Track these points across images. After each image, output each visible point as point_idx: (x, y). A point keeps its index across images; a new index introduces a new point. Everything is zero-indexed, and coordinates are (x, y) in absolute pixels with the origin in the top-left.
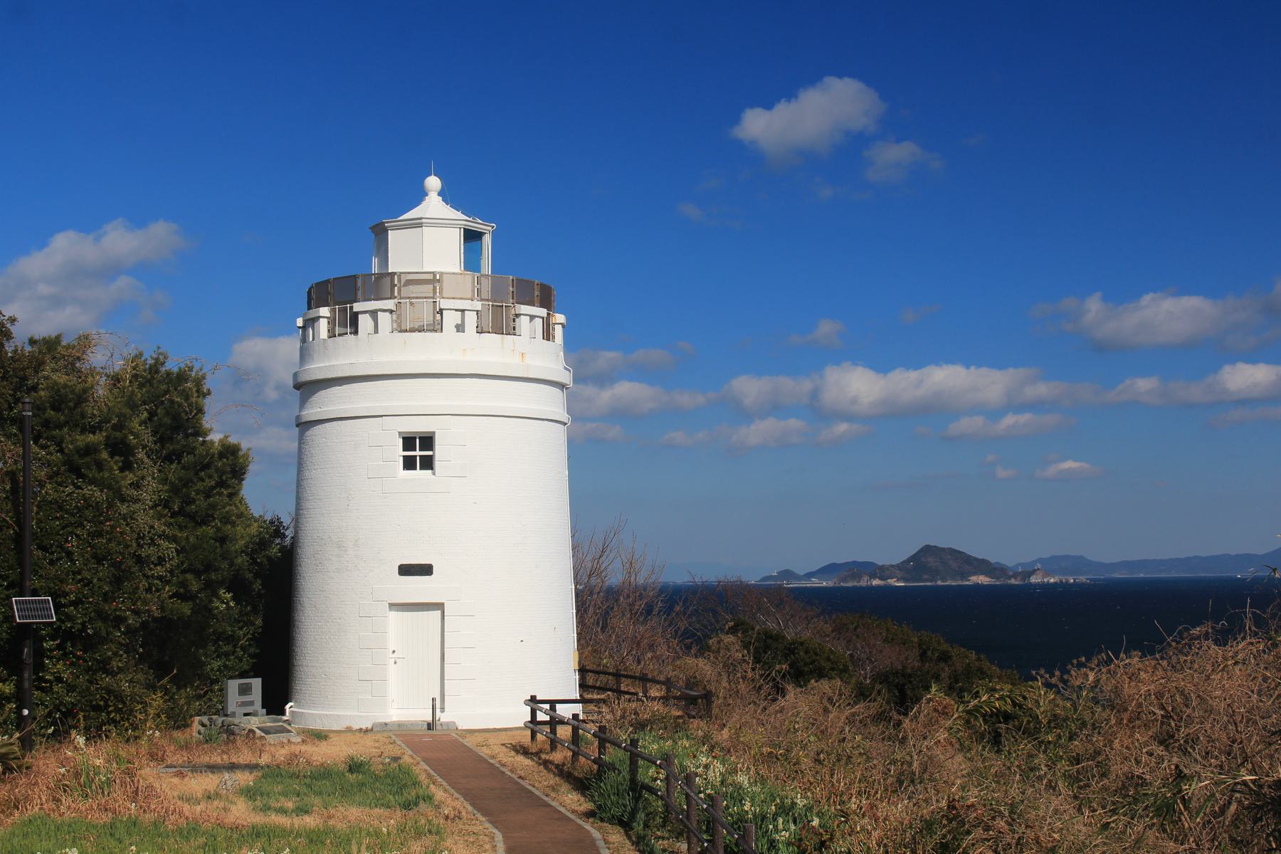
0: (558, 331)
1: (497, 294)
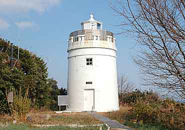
0: (114, 41)
1: (103, 32)
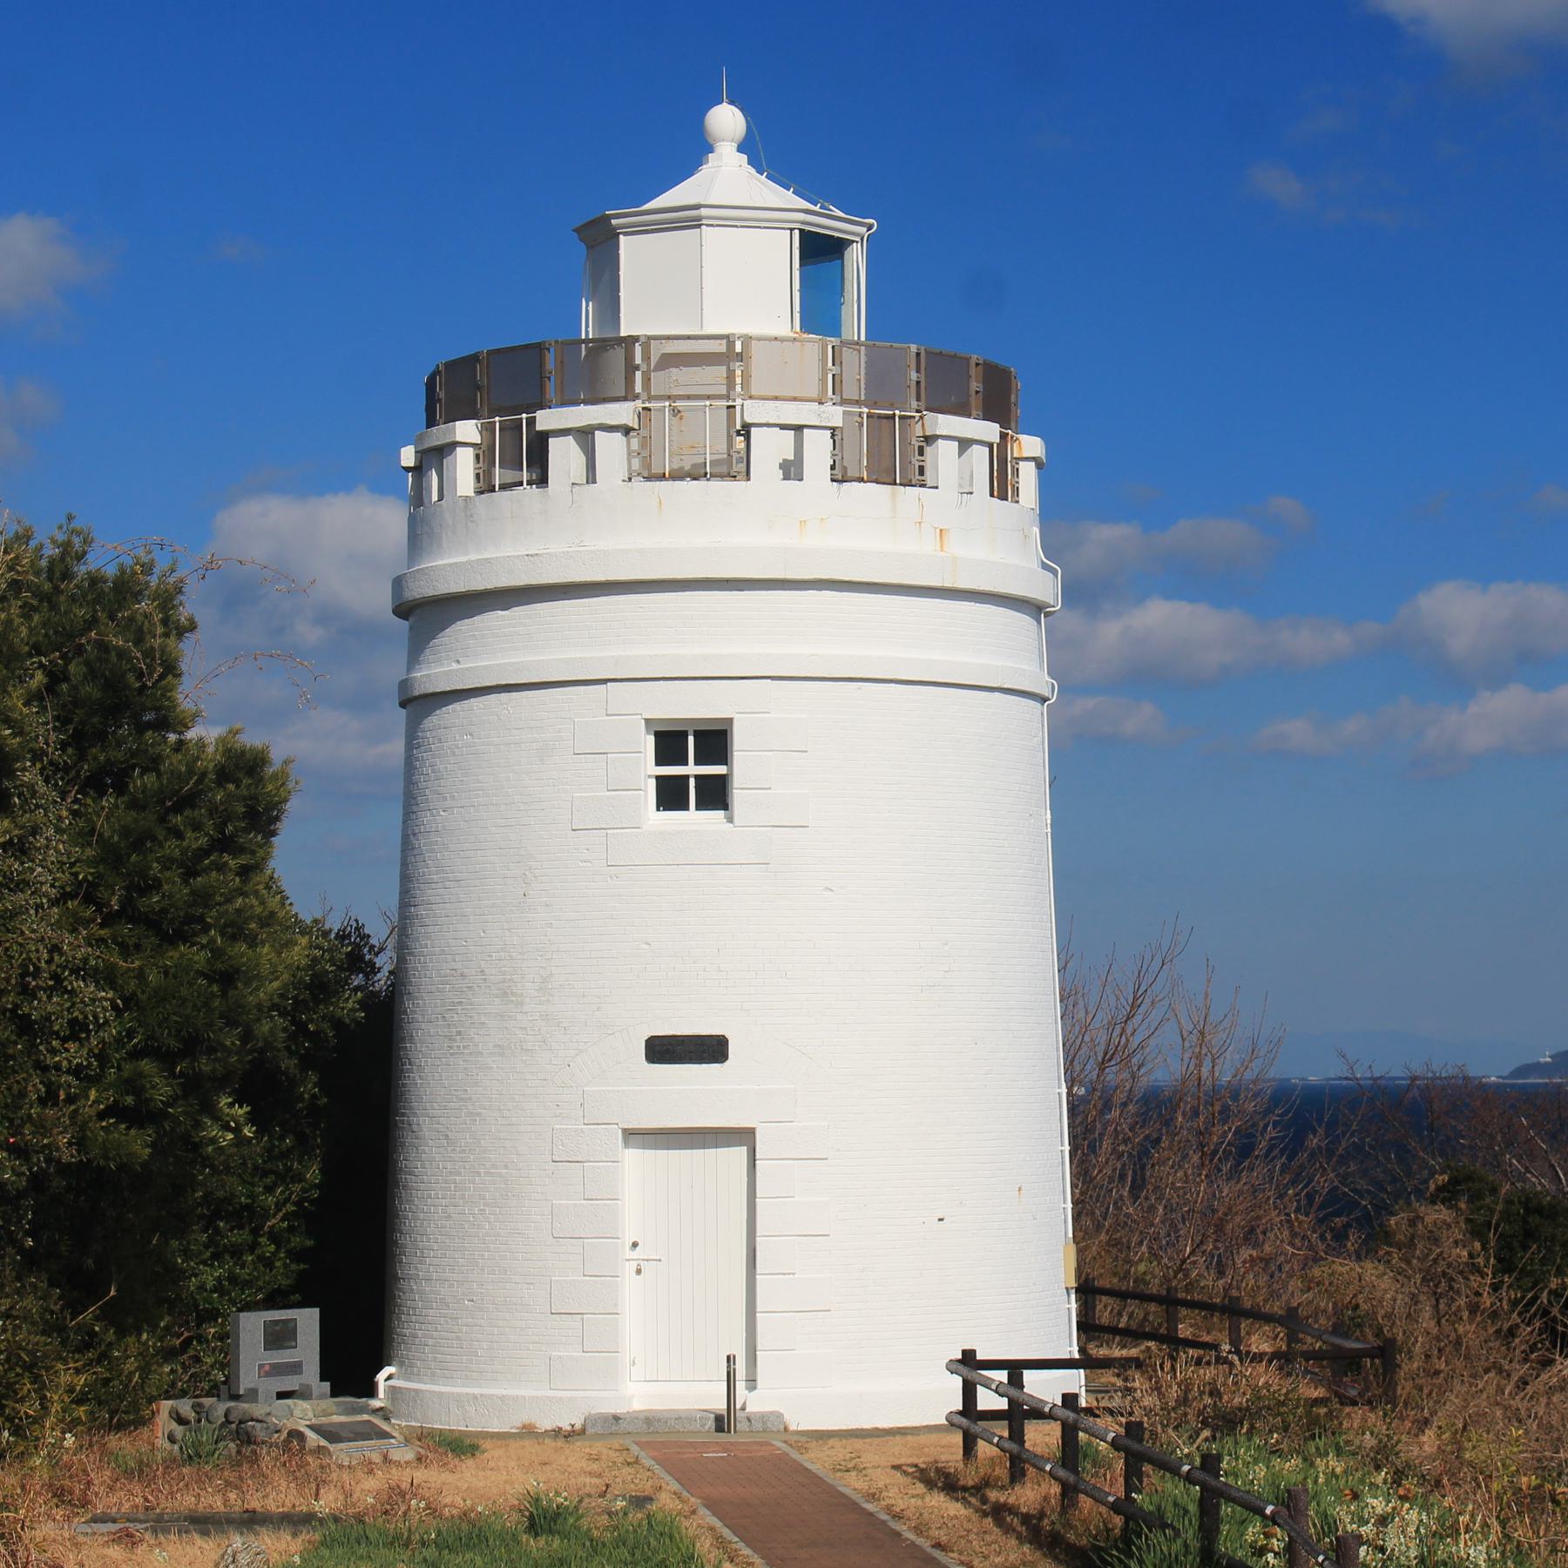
0: (1028, 477)
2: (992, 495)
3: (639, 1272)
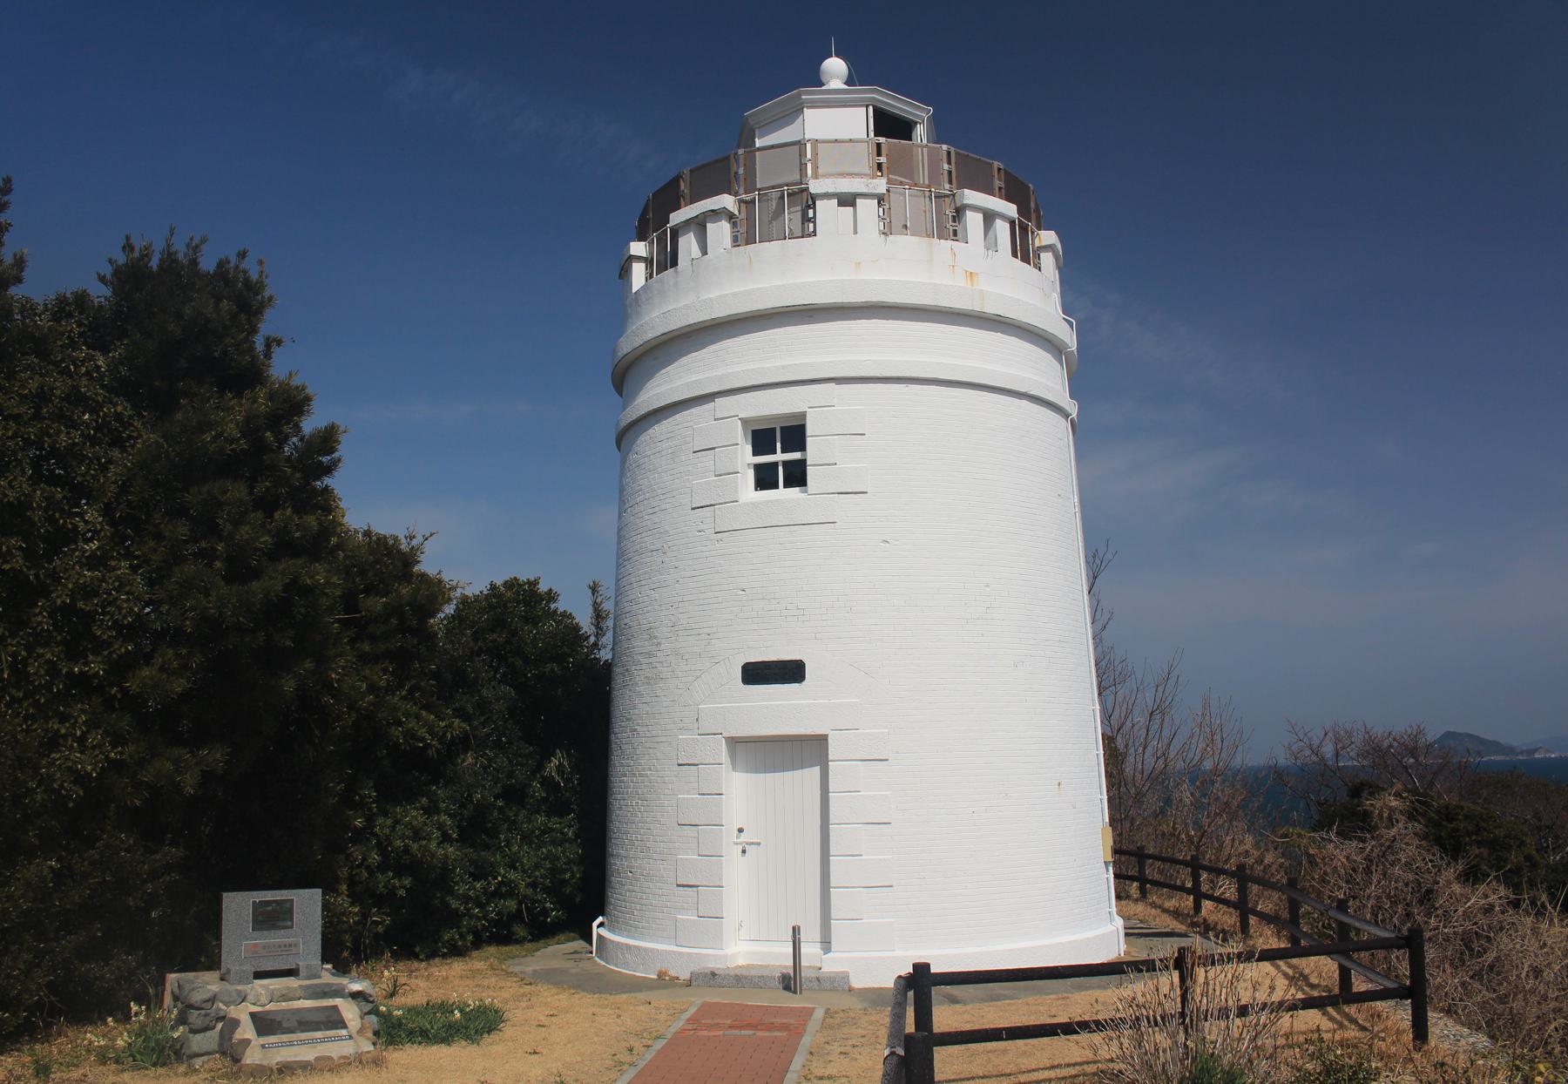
2: (1015, 255)
3: (744, 851)
